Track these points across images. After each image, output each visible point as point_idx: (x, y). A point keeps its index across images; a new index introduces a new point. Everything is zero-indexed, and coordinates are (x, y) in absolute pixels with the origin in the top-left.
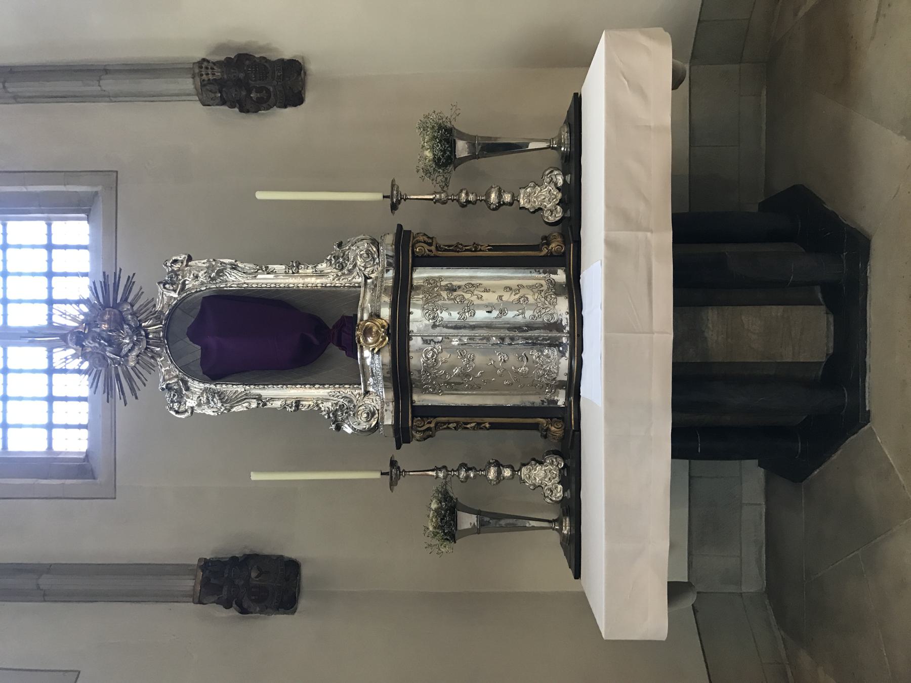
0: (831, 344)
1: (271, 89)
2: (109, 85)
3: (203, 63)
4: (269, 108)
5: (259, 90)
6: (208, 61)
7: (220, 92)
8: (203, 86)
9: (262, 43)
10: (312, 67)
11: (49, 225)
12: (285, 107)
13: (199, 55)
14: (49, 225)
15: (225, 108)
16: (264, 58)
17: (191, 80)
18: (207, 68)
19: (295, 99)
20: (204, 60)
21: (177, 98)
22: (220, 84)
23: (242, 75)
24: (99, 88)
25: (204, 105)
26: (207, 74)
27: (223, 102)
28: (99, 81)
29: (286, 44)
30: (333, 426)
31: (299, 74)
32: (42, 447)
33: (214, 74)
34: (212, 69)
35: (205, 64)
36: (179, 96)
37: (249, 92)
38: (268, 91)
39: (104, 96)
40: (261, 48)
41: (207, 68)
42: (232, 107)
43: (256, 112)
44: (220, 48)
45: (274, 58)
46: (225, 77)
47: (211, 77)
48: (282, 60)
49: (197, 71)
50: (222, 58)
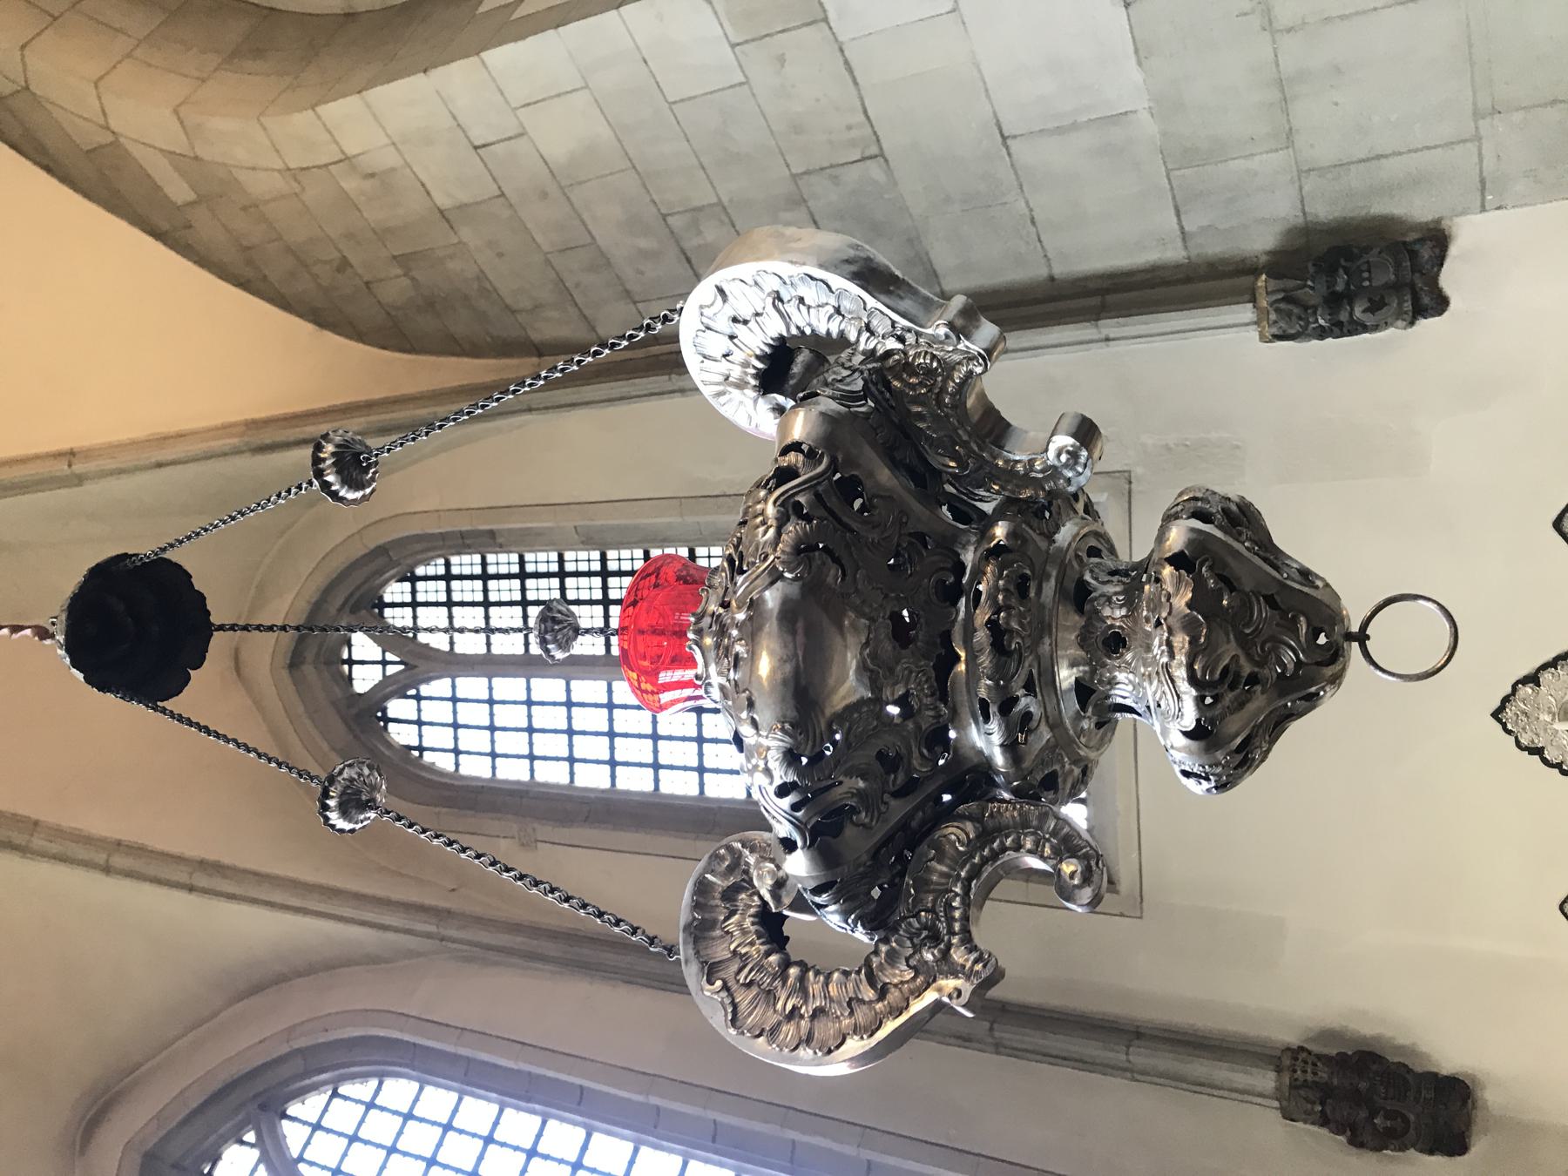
0: (627, 1132)
1: (1412, 1118)
2: (1141, 1057)
3: (1297, 1052)
4: (1403, 1148)
5: (1389, 1115)
6: (1310, 1053)
7: (1322, 1103)
8: (1294, 1086)
9: (1401, 1040)
10: (1491, 1098)
11: (589, 1136)
12: (1431, 1152)
13: (1292, 1039)
14: (589, 1136)
15: (1324, 1131)
16: (1405, 1066)
17: (1272, 1075)
18: (1306, 1062)
19: (1453, 1142)
20: (1301, 1049)
21: (1240, 1097)
22: (1325, 1093)
23: (1363, 1085)
24: (1124, 1057)
25: (1285, 1117)
26: (1305, 1072)
27: (1324, 1122)
28: (1128, 1047)
29: (1449, 1051)
30: (273, 765)
31: (1465, 1102)
32: (694, 791)
33: (1315, 1074)
34: (1315, 1065)
35: (1304, 1055)
36: (1245, 1093)
37: (1373, 1114)
38: (1406, 1120)
39: (1125, 1070)
40: (1401, 1049)
41: (1306, 1062)
42: (1338, 1131)
43: (1378, 1149)
44: (1328, 1035)
45: (1419, 1069)
46: (1335, 1082)
47: (1309, 1077)
48: (1435, 1075)
49: (1287, 1062)
50: (1334, 1052)
